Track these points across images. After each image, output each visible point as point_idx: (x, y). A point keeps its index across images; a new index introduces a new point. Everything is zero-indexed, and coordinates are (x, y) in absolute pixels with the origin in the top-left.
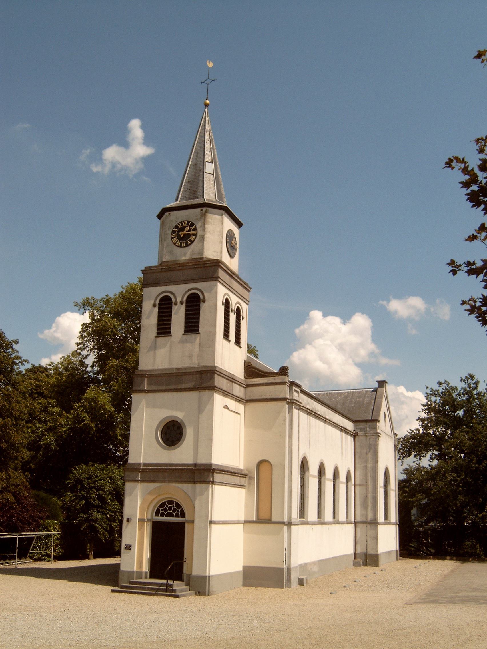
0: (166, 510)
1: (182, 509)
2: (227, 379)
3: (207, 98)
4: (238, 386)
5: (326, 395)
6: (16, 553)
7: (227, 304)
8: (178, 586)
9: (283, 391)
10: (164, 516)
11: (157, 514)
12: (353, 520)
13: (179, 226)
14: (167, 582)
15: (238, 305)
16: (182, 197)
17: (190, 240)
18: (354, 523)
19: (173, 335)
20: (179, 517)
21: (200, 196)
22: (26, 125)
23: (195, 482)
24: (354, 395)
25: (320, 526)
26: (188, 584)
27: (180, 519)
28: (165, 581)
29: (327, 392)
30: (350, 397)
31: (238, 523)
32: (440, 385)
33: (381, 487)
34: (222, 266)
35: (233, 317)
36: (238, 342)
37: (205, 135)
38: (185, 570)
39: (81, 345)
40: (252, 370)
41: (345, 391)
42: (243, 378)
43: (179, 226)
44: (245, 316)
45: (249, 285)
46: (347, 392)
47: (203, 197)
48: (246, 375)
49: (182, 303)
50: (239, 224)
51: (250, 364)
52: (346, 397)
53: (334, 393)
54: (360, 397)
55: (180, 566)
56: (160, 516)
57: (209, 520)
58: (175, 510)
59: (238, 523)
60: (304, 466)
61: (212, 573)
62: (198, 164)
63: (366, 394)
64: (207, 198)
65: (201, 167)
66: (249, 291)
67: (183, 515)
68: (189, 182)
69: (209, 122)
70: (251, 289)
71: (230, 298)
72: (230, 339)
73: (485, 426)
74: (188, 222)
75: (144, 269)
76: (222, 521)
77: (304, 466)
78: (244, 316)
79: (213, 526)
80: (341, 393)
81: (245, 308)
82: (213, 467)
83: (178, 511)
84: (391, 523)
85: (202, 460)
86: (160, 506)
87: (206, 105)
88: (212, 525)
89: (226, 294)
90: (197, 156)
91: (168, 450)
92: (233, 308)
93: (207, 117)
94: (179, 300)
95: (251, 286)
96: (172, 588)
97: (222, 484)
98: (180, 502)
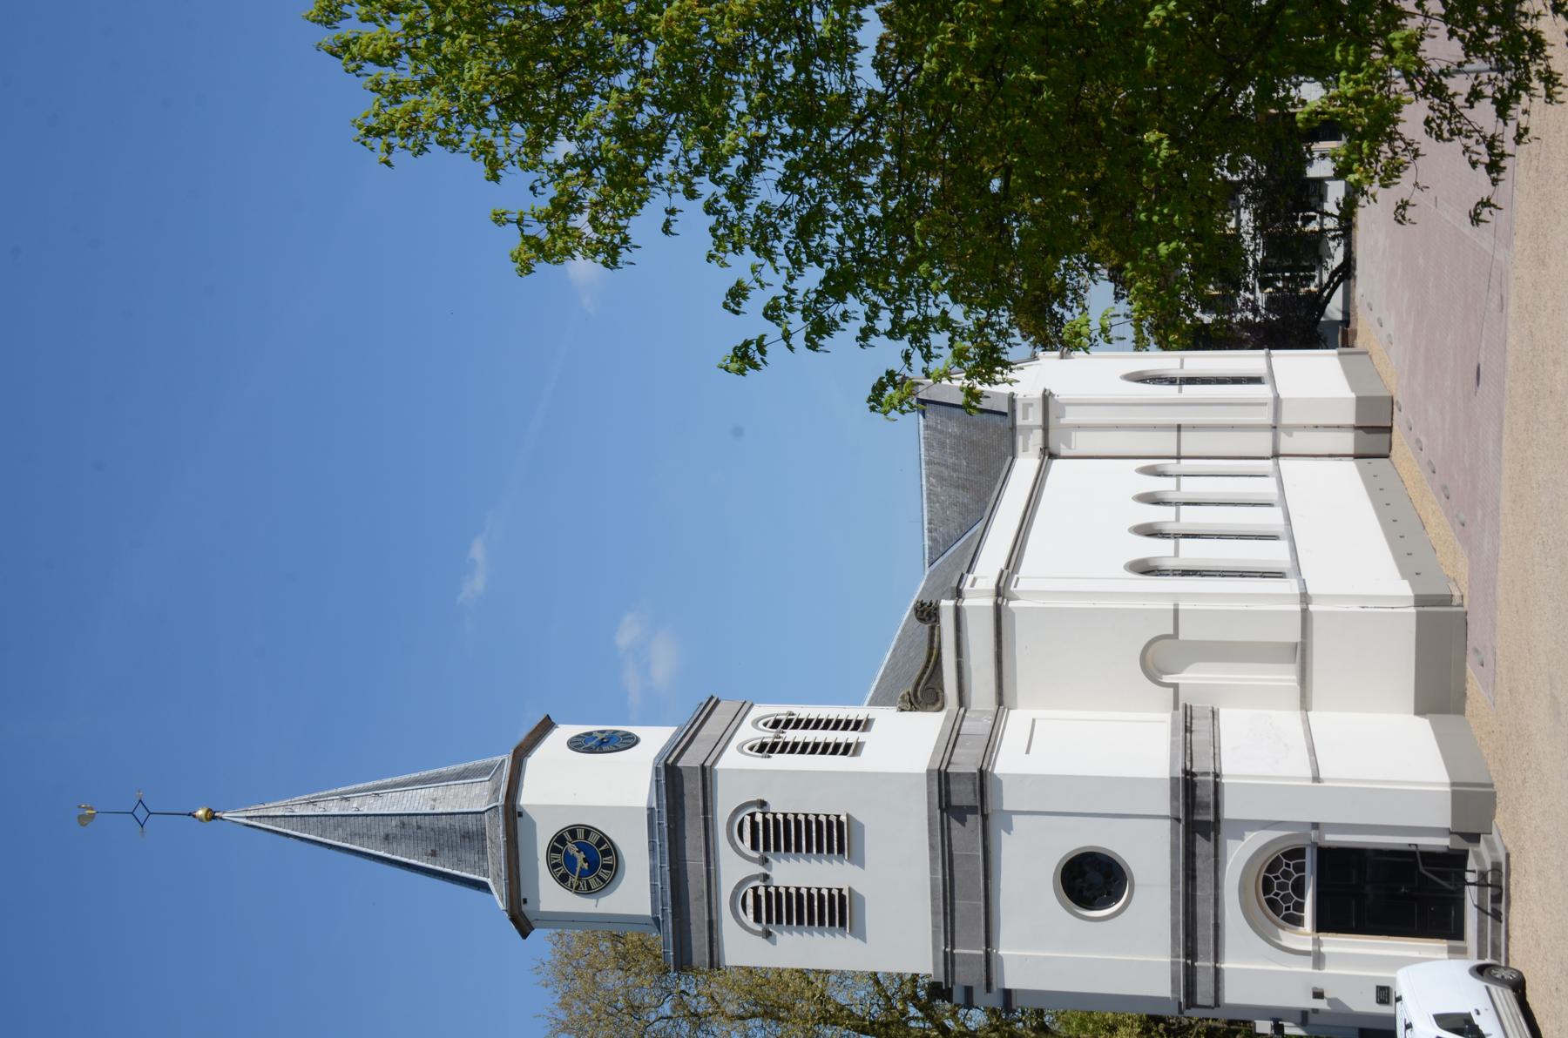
1: (1283, 854)
3: (190, 814)
5: (934, 534)
7: (764, 749)
8: (1478, 856)
12: (1270, 462)
15: (760, 725)
16: (477, 870)
21: (479, 823)
24: (936, 461)
26: (1474, 838)
27: (1310, 861)
28: (1471, 895)
29: (926, 532)
30: (943, 469)
31: (1306, 722)
32: (392, 15)
33: (1180, 391)
34: (671, 759)
35: (791, 735)
37: (301, 816)
38: (1442, 843)
40: (922, 692)
41: (924, 483)
42: (943, 714)
46: (928, 477)
47: (483, 813)
48: (934, 704)
50: (546, 726)
51: (907, 697)
52: (941, 479)
53: (930, 511)
54: (942, 445)
55: (1431, 857)
57: (1310, 783)
59: (1306, 722)
61: (1447, 780)
62: (386, 831)
63: (935, 429)
64: (484, 804)
65: (394, 823)
66: (718, 702)
68: (434, 854)
69: (262, 806)
70: (712, 697)
76: (1310, 756)
77: (1146, 569)
79: (1322, 775)
85: (1163, 803)
87: (212, 816)
89: (740, 748)
90: (361, 836)
93: (248, 814)
96: (1490, 874)
97: (1216, 757)
98: (1268, 859)
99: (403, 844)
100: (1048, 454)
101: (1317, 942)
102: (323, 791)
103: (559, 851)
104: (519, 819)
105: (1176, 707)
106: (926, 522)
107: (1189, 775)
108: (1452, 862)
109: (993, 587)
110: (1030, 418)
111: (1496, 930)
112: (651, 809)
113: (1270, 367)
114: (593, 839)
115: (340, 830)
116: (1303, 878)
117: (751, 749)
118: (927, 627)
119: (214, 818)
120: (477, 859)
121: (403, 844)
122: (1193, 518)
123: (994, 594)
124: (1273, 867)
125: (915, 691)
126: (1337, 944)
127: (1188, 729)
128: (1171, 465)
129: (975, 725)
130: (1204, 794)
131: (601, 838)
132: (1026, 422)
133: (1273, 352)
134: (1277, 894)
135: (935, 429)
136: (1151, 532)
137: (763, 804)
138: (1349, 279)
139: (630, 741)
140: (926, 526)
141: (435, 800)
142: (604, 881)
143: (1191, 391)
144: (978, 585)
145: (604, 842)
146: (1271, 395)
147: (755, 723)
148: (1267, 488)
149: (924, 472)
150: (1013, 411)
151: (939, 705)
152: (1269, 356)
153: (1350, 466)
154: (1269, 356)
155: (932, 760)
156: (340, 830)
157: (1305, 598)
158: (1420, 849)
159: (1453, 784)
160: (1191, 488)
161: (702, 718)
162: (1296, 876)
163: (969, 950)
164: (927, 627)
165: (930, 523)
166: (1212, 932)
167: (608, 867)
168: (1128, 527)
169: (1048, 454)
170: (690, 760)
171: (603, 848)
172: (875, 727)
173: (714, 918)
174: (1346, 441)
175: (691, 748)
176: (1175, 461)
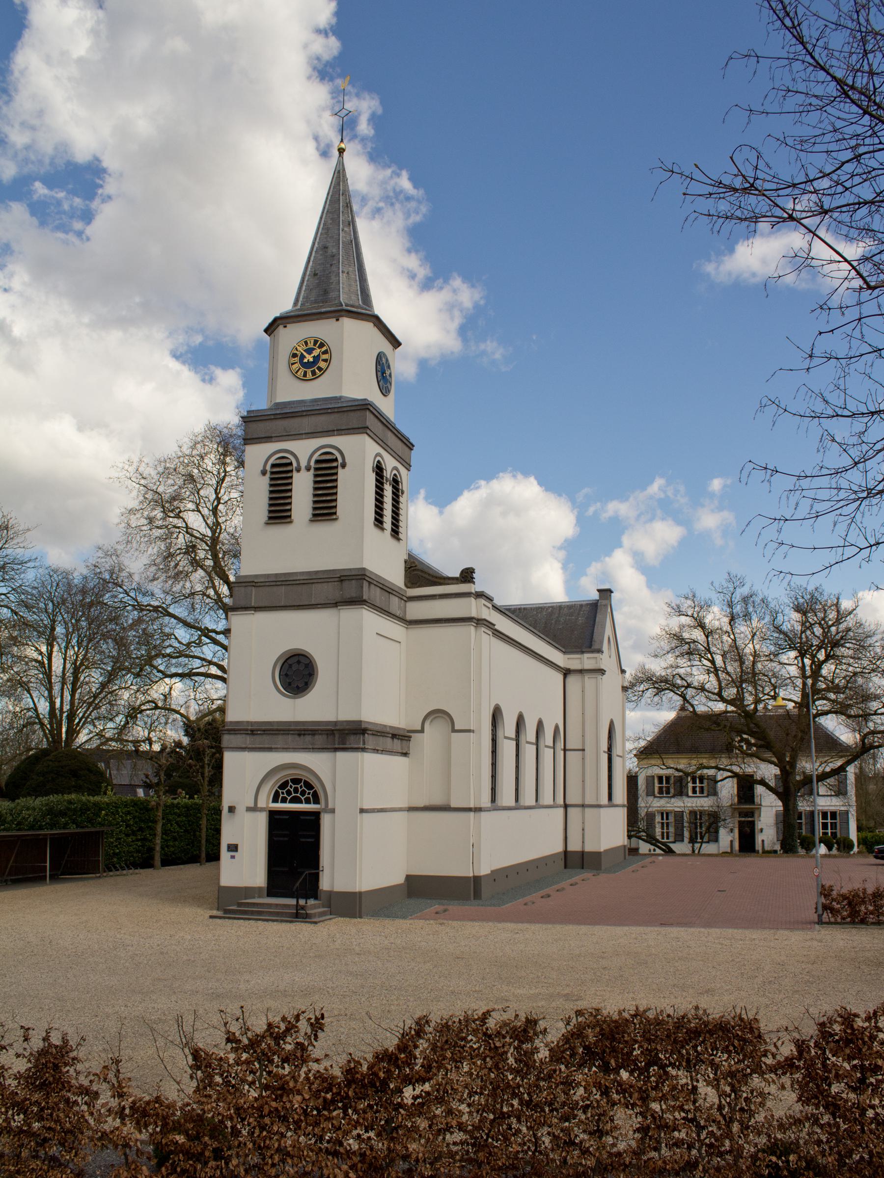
0: (289, 793)
4: (397, 599)
7: (379, 470)
8: (314, 907)
9: (474, 607)
11: (275, 800)
12: (562, 803)
14: (298, 902)
15: (395, 472)
17: (320, 369)
19: (295, 521)
22: (586, 490)
27: (311, 807)
28: (293, 902)
35: (388, 490)
39: (130, 535)
42: (403, 587)
45: (411, 441)
48: (410, 581)
49: (308, 469)
54: (571, 615)
55: (315, 878)
58: (303, 793)
60: (496, 715)
63: (580, 610)
67: (317, 800)
68: (315, 275)
72: (385, 525)
73: (880, 1166)
74: (316, 342)
75: (245, 414)
77: (496, 715)
82: (363, 726)
85: (346, 715)
91: (295, 698)
94: (303, 464)
97: (376, 751)
100: (567, 673)
101: (261, 810)
105: (409, 731)
107: (364, 731)
108: (311, 889)
109: (484, 617)
110: (587, 661)
111: (286, 915)
112: (340, 398)
113: (617, 806)
114: (322, 365)
116: (301, 802)
117: (379, 462)
118: (458, 575)
122: (529, 752)
123: (479, 617)
124: (309, 786)
125: (418, 570)
126: (261, 821)
127: (394, 736)
128: (560, 745)
129: (395, 604)
130: (352, 740)
132: (586, 660)
133: (626, 809)
134: (309, 794)
135: (580, 610)
136: (520, 722)
137: (344, 466)
139: (385, 391)
141: (348, 273)
142: (297, 372)
143: (605, 757)
144: (484, 609)
146: (602, 803)
147: (395, 468)
148: (547, 799)
150: (593, 652)
151: (409, 585)
152: (623, 806)
153: (560, 848)
154: (623, 806)
155: (371, 572)
157: (478, 810)
158: (321, 873)
159: (360, 893)
160: (547, 754)
164: (458, 575)
166: (267, 746)
167: (305, 374)
169: (567, 673)
170: (370, 421)
172: (393, 542)
173: (370, 741)
174: (574, 846)
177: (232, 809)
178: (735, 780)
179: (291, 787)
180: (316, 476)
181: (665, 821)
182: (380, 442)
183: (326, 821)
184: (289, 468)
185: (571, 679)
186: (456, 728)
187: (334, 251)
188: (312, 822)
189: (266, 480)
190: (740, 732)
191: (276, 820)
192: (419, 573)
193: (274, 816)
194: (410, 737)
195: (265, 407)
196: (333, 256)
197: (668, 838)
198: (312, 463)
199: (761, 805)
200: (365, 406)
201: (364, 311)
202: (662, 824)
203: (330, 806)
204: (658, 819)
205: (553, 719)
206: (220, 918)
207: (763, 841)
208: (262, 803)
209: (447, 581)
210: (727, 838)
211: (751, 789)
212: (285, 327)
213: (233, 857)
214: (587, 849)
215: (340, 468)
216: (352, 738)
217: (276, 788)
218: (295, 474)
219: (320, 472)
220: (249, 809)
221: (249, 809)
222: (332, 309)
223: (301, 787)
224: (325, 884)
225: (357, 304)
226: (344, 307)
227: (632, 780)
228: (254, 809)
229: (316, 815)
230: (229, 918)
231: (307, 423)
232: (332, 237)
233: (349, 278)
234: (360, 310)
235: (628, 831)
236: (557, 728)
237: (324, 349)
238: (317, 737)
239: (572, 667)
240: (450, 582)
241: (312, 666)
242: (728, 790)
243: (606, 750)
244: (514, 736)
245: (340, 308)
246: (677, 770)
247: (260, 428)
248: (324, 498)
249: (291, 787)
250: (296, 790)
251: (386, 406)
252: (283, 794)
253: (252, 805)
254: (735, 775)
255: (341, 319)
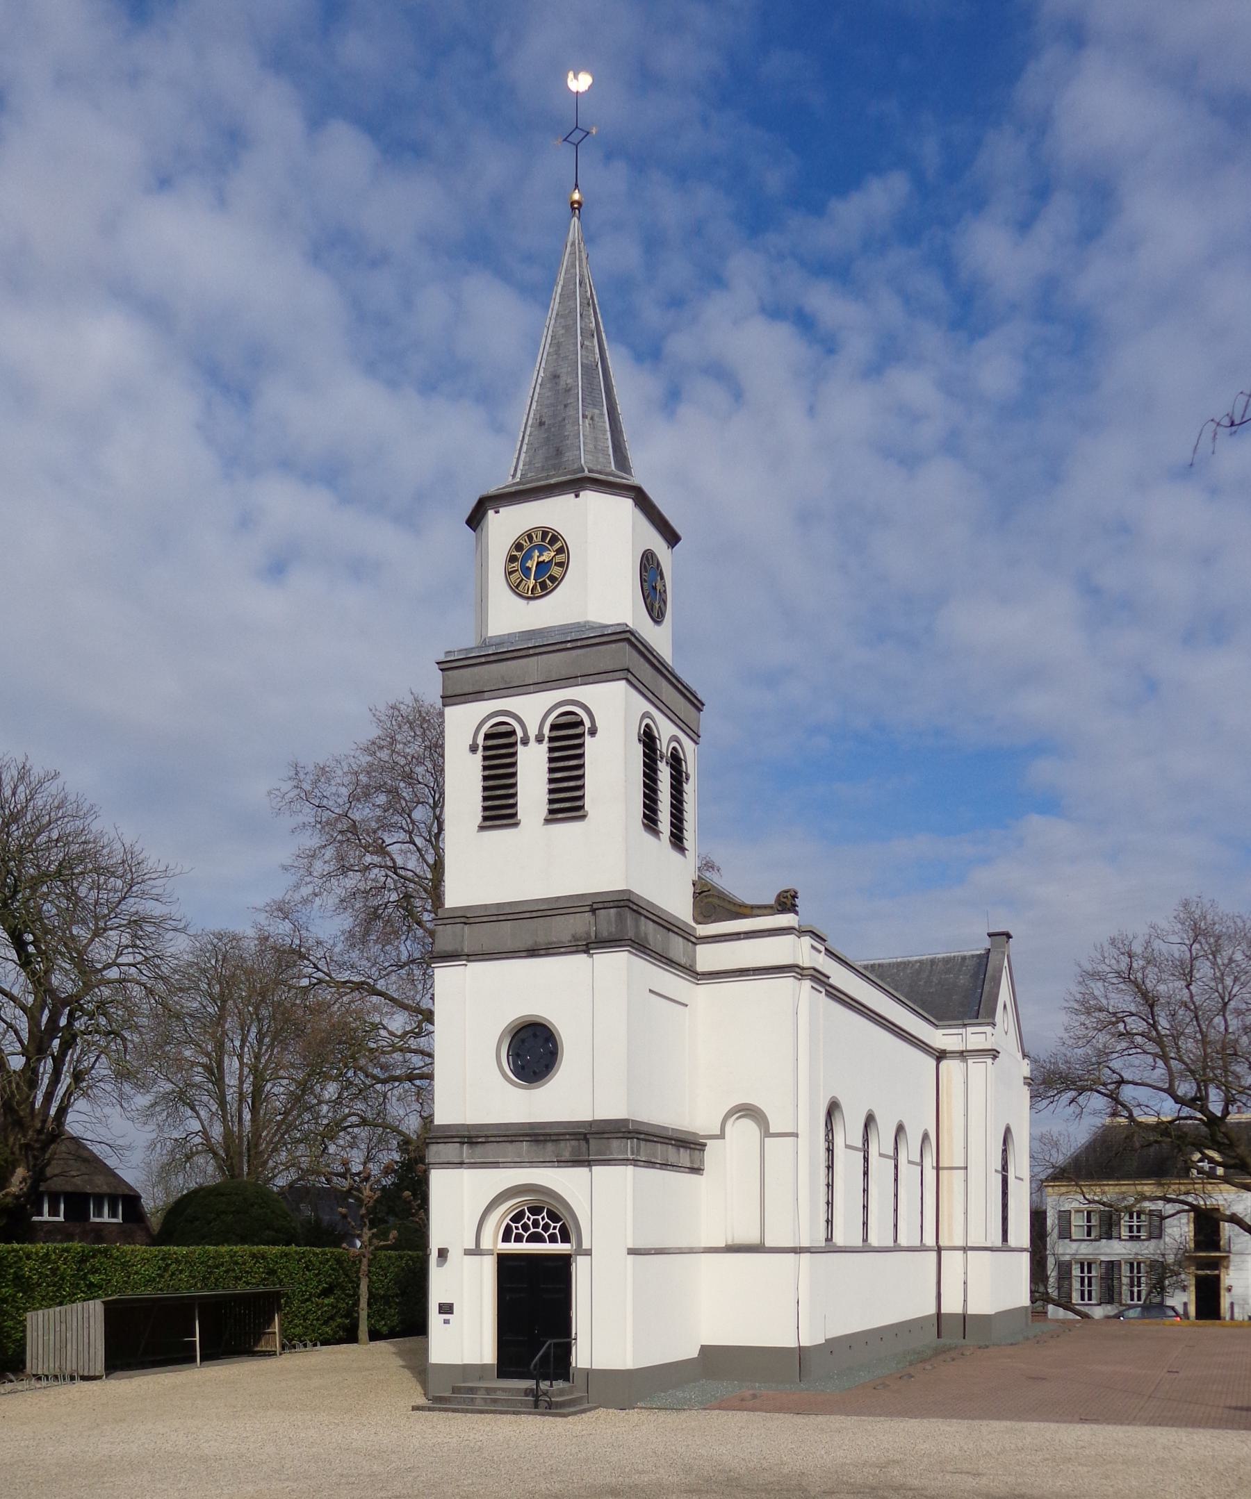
2: (654, 921)
4: (681, 939)
6: (195, 1337)
7: (648, 739)
10: (510, 1242)
11: (506, 1238)
13: (525, 544)
15: (674, 744)
16: (527, 467)
18: (936, 1248)
20: (557, 1242)
23: (588, 1163)
25: (793, 1254)
27: (560, 1247)
29: (872, 962)
35: (664, 773)
36: (677, 839)
43: (525, 544)
44: (691, 771)
49: (539, 740)
50: (672, 538)
52: (919, 972)
55: (565, 1351)
56: (515, 1241)
68: (541, 424)
70: (703, 705)
71: (654, 723)
74: (545, 534)
78: (689, 772)
80: (878, 977)
81: (689, 750)
83: (555, 1228)
84: (925, 1246)
86: (514, 1219)
88: (961, 1312)
89: (646, 715)
92: (664, 751)
94: (533, 732)
95: (703, 700)
98: (561, 1212)
99: (550, 394)
101: (490, 1252)
102: (602, 317)
103: (543, 539)
104: (573, 495)
106: (880, 961)
110: (975, 1037)
114: (556, 571)
115: (563, 332)
117: (647, 726)
119: (573, 209)
120: (536, 465)
121: (550, 394)
122: (881, 1169)
124: (554, 1217)
126: (487, 1269)
128: (929, 1162)
129: (677, 947)
131: (556, 579)
137: (593, 732)
138: (1216, 1215)
139: (657, 616)
140: (877, 962)
141: (592, 418)
142: (517, 587)
145: (553, 583)
147: (675, 738)
149: (924, 957)
151: (700, 919)
156: (563, 332)
161: (680, 686)
162: (546, 1235)
163: (469, 937)
165: (879, 965)
168: (874, 1110)
171: (548, 581)
172: (675, 855)
174: (952, 1306)
175: (647, 665)
176: (935, 1165)
177: (443, 1253)
178: (1192, 1214)
179: (529, 1218)
180: (551, 750)
181: (1086, 1274)
182: (650, 695)
183: (580, 1270)
184: (511, 740)
185: (944, 1064)
186: (772, 1130)
187: (569, 381)
188: (560, 1268)
189: (477, 760)
190: (1199, 1147)
191: (508, 1267)
192: (716, 901)
193: (504, 1260)
194: (705, 1145)
195: (473, 645)
196: (569, 390)
197: (1090, 1299)
198: (546, 731)
199: (1229, 1252)
200: (626, 637)
201: (618, 480)
202: (1082, 1279)
203: (586, 1245)
204: (1076, 1271)
205: (920, 1122)
206: (430, 1409)
207: (1232, 1304)
208: (486, 1244)
209: (756, 911)
210: (1182, 1299)
211: (1216, 1231)
212: (497, 512)
213: (446, 1322)
214: (971, 1310)
215: (587, 737)
216: (615, 1144)
217: (507, 1220)
218: (520, 748)
219: (557, 754)
220: (468, 1252)
221: (468, 1252)
222: (569, 477)
223: (543, 1218)
224: (581, 1358)
225: (608, 470)
226: (586, 473)
227: (1038, 1218)
228: (477, 1251)
229: (564, 1263)
230: (440, 1410)
231: (533, 667)
232: (566, 358)
233: (593, 426)
234: (611, 479)
235: (1032, 1292)
236: (926, 1137)
237: (560, 558)
238: (562, 1144)
239: (949, 1048)
240: (758, 912)
241: (555, 1038)
242: (1180, 1230)
243: (1000, 1168)
244: (860, 1145)
245: (579, 475)
246: (1104, 1204)
247: (466, 678)
248: (565, 785)
249: (529, 1218)
250: (536, 1223)
251: (659, 638)
252: (517, 1229)
253: (473, 1246)
254: (1194, 1208)
255: (582, 494)
